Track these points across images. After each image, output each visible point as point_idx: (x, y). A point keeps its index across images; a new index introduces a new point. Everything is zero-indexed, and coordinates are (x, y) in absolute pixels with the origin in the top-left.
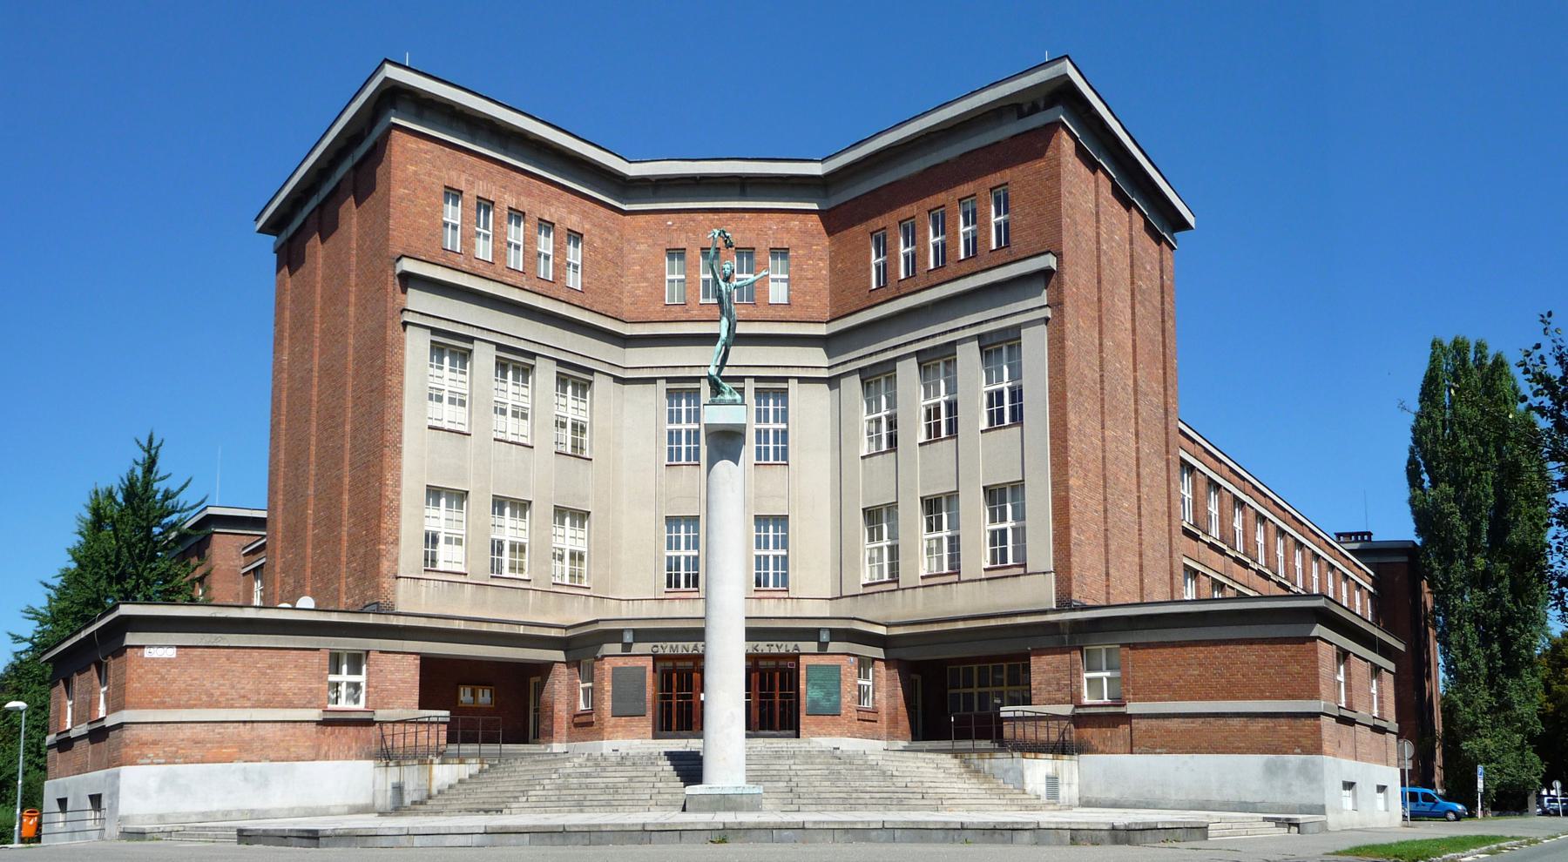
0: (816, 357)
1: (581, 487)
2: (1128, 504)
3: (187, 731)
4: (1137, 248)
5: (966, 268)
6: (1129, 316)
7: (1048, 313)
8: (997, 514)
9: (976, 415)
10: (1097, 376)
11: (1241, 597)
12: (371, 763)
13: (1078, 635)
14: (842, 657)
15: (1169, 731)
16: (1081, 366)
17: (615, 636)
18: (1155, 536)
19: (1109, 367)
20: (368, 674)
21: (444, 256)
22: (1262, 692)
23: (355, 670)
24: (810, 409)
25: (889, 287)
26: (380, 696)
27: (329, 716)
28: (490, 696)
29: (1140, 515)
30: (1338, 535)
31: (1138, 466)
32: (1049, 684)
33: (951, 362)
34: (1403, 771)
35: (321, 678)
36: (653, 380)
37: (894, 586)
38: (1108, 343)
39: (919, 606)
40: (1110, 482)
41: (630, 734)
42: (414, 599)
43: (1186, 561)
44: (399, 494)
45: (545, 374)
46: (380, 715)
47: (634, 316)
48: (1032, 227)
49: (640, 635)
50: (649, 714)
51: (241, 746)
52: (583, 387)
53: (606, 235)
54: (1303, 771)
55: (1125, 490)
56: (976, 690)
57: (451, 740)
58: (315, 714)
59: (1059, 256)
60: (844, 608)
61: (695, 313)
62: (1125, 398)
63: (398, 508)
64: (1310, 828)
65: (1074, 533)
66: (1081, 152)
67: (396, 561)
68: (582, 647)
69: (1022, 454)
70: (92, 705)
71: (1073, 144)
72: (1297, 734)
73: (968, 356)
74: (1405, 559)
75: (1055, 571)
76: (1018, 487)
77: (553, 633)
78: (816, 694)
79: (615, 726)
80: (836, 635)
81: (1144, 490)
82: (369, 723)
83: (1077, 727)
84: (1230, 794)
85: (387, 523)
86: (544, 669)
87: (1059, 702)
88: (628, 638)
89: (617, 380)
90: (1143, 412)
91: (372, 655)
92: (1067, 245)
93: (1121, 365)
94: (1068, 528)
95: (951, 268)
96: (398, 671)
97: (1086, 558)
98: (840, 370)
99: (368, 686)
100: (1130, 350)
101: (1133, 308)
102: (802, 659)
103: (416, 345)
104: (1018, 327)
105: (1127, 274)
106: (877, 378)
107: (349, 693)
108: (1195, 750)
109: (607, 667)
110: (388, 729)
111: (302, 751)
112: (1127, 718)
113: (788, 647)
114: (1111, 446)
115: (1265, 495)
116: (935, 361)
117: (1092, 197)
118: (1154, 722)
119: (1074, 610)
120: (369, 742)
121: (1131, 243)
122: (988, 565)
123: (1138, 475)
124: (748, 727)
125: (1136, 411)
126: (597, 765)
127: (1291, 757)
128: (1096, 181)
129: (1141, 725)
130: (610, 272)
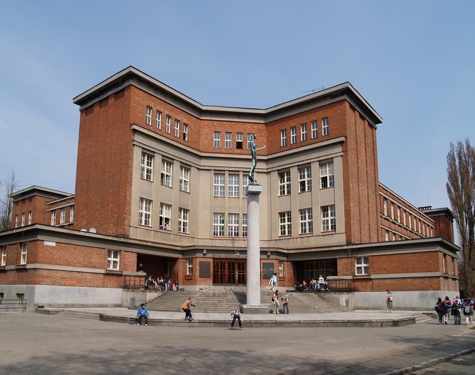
1: (188, 203)
2: (366, 210)
4: (366, 131)
5: (314, 141)
6: (364, 152)
7: (342, 154)
8: (325, 215)
10: (356, 171)
11: (407, 239)
12: (121, 289)
13: (354, 252)
15: (385, 284)
16: (353, 169)
18: (373, 219)
19: (360, 168)
20: (120, 258)
21: (146, 126)
22: (418, 270)
23: (115, 256)
24: (262, 183)
25: (288, 146)
27: (108, 272)
28: (158, 266)
29: (369, 213)
30: (419, 208)
31: (368, 197)
32: (344, 269)
35: (105, 259)
37: (290, 237)
38: (360, 161)
40: (361, 203)
41: (205, 283)
42: (136, 234)
44: (131, 199)
45: (177, 165)
46: (125, 273)
47: (203, 150)
48: (336, 129)
49: (209, 251)
50: (212, 277)
52: (187, 170)
53: (195, 126)
55: (365, 205)
58: (103, 271)
59: (346, 137)
60: (272, 244)
61: (223, 151)
62: (364, 177)
63: (130, 203)
65: (352, 221)
66: (351, 106)
67: (130, 221)
68: (190, 253)
69: (335, 195)
70: (18, 259)
75: (346, 233)
76: (333, 207)
77: (179, 248)
79: (200, 280)
80: (272, 253)
81: (370, 204)
82: (121, 275)
83: (353, 282)
85: (127, 208)
86: (175, 260)
87: (347, 275)
89: (198, 169)
90: (369, 179)
91: (122, 252)
92: (348, 134)
93: (363, 167)
94: (350, 219)
95: (309, 141)
96: (131, 258)
97: (355, 228)
98: (270, 170)
99: (120, 262)
100: (365, 161)
101: (366, 149)
103: (137, 152)
105: (364, 139)
106: (283, 174)
107: (114, 263)
109: (197, 261)
110: (128, 278)
111: (99, 284)
112: (371, 279)
114: (361, 192)
115: (400, 200)
117: (354, 119)
118: (380, 281)
119: (353, 245)
120: (121, 282)
121: (365, 130)
123: (368, 200)
125: (367, 180)
126: (206, 296)
128: (355, 114)
129: (376, 282)
130: (196, 136)
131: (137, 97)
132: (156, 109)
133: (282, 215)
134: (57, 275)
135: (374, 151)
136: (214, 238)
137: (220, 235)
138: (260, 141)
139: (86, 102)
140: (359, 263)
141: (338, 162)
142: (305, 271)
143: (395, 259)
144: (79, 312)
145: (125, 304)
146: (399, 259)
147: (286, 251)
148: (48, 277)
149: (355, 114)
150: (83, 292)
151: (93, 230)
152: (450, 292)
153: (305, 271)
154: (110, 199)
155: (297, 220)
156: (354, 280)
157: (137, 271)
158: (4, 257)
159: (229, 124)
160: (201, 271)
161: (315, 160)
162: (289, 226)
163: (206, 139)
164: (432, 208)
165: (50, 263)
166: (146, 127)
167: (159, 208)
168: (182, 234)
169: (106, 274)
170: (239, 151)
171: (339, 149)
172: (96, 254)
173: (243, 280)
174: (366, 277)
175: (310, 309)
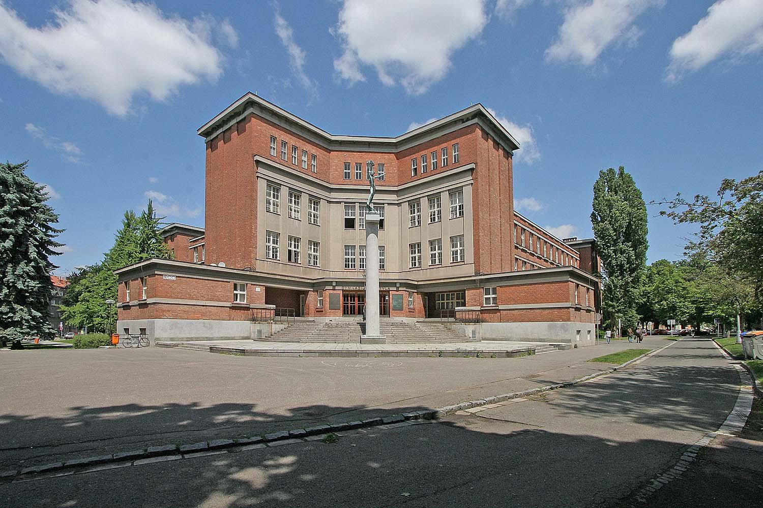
0: (393, 197)
3: (182, 307)
9: (447, 214)
14: (403, 292)
17: (330, 283)
26: (251, 299)
28: (288, 301)
30: (564, 240)
33: (439, 199)
34: (596, 325)
36: (340, 202)
39: (428, 276)
42: (263, 267)
43: (516, 256)
51: (203, 313)
54: (562, 327)
56: (445, 301)
57: (277, 314)
60: (403, 276)
64: (566, 348)
68: (319, 286)
69: (465, 226)
70: (140, 294)
72: (560, 315)
73: (445, 197)
74: (590, 245)
79: (330, 312)
80: (402, 285)
81: (502, 234)
82: (248, 309)
84: (535, 336)
88: (334, 284)
89: (329, 202)
97: (484, 258)
103: (262, 185)
104: (462, 187)
106: (414, 205)
116: (434, 199)
122: (452, 262)
124: (381, 314)
126: (329, 327)
129: (505, 312)
131: (256, 126)
132: (281, 139)
133: (412, 246)
134: (179, 309)
136: (346, 270)
137: (352, 267)
139: (213, 135)
140: (487, 293)
141: (468, 192)
142: (437, 302)
144: (196, 345)
145: (252, 336)
147: (416, 283)
148: (169, 311)
150: (208, 326)
151: (222, 264)
153: (437, 302)
154: (238, 232)
155: (426, 251)
156: (482, 311)
158: (145, 290)
160: (330, 303)
161: (445, 189)
162: (420, 258)
165: (171, 297)
166: (270, 158)
167: (288, 242)
168: (312, 267)
169: (232, 308)
170: (347, 181)
172: (224, 288)
173: (361, 311)
174: (494, 308)
175: (435, 337)
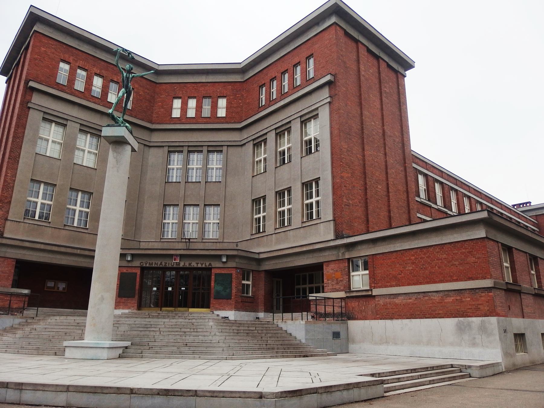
15: (396, 305)
22: (451, 277)
30: (514, 206)
71: (343, 32)
78: (219, 288)
102: (213, 271)
108: (412, 316)
113: (206, 264)
127: (474, 319)
135: (400, 106)
138: (235, 105)
143: (410, 259)
146: (416, 259)
149: (358, 48)
152: (527, 321)
157: (12, 287)
159: (193, 87)
161: (296, 116)
163: (162, 107)
164: (532, 204)
171: (325, 93)
